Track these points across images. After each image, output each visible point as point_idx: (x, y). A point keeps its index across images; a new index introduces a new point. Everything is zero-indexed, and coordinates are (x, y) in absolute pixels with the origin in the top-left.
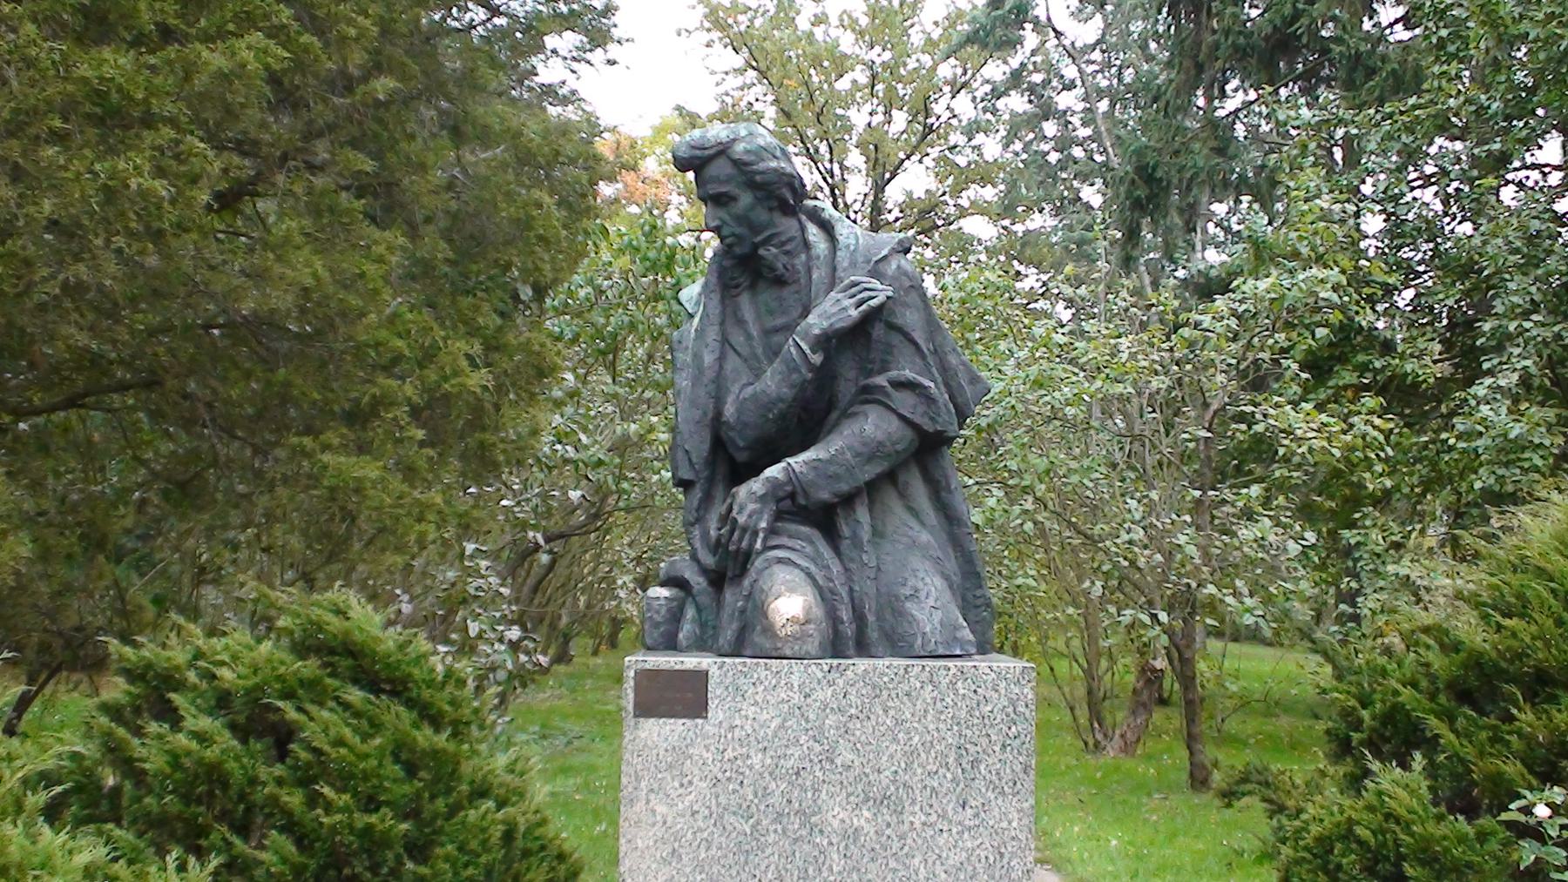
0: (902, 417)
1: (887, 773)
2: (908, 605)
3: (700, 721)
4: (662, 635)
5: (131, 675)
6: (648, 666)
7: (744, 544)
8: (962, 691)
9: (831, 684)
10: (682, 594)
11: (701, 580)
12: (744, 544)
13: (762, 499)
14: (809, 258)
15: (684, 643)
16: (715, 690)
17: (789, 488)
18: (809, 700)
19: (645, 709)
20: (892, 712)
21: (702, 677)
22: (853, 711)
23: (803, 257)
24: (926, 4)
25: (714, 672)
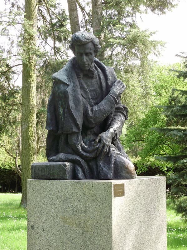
8: (158, 184)
9: (141, 185)
10: (72, 164)
12: (108, 150)
16: (126, 189)
19: (116, 195)
21: (123, 185)
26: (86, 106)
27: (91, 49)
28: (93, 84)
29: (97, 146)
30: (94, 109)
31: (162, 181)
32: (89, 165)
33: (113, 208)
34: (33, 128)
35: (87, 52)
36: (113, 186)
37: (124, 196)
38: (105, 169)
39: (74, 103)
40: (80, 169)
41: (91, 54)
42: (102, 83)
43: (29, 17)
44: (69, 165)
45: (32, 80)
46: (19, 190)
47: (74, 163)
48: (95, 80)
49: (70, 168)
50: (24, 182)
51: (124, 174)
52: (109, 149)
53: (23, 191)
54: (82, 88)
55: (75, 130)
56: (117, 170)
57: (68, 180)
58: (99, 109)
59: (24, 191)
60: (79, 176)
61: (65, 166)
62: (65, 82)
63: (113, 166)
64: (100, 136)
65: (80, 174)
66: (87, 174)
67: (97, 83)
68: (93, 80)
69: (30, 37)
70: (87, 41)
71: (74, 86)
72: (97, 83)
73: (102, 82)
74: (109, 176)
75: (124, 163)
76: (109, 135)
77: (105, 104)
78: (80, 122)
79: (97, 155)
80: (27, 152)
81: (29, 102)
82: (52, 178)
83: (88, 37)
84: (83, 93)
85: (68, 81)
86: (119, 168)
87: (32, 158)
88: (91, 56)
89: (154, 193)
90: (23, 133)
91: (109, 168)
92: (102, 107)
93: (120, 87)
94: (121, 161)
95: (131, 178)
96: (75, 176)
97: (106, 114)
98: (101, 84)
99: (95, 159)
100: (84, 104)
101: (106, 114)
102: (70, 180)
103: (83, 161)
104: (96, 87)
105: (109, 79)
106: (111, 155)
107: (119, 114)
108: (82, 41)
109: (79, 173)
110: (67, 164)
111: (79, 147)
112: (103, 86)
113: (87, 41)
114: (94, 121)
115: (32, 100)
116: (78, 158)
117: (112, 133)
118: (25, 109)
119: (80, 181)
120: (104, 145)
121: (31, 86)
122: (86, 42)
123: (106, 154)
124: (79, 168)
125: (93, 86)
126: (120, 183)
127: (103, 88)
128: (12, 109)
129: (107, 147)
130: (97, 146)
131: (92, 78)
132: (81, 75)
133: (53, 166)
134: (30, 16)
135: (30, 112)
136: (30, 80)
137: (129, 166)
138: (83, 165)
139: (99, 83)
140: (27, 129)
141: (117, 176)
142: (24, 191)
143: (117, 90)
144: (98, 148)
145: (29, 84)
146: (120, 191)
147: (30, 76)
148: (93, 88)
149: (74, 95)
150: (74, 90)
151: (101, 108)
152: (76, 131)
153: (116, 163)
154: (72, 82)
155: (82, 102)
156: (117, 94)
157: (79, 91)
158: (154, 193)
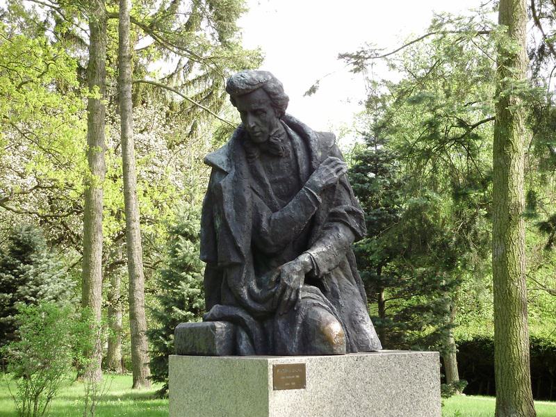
0: (353, 230)
1: (382, 410)
2: (362, 325)
3: (302, 390)
4: (224, 348)
5: (43, 257)
6: (496, 371)
7: (292, 297)
8: (411, 367)
9: (358, 366)
10: (231, 325)
11: (249, 316)
12: (292, 297)
13: (299, 273)
14: (293, 144)
15: (245, 351)
16: (308, 374)
17: (311, 267)
18: (349, 375)
19: (279, 385)
20: (384, 379)
21: (302, 367)
22: (368, 380)
23: (289, 143)
24: (3, 410)
25: (308, 365)
26: (260, 212)
27: (261, 101)
28: (281, 168)
29: (273, 290)
30: (273, 218)
31: (427, 362)
32: (263, 328)
33: (270, 411)
34: (516, 255)
35: (253, 108)
36: (272, 368)
37: (304, 388)
38: (284, 335)
39: (235, 208)
40: (244, 335)
41: (264, 112)
42: (298, 165)
43: (508, 16)
44: (221, 328)
45: (514, 150)
46: (490, 392)
47: (234, 321)
48: (285, 160)
49: (225, 333)
50: (499, 372)
51: (318, 345)
52: (297, 295)
53: (497, 394)
54: (256, 176)
55: (235, 259)
56: (307, 338)
57: (218, 356)
58: (281, 216)
59: (499, 394)
60: (239, 348)
61: (214, 328)
62: (221, 167)
63: (298, 328)
64: (280, 270)
65: (244, 344)
66: (258, 345)
67: (290, 166)
68: (282, 162)
69: (507, 58)
70: (250, 87)
71: (236, 175)
72: (290, 166)
73: (300, 164)
74: (289, 348)
75: (320, 324)
76: (298, 268)
77: (294, 206)
78: (244, 243)
79: (275, 307)
80: (504, 307)
81: (507, 199)
82: (197, 352)
83: (252, 81)
84: (256, 187)
85: (228, 166)
86: (310, 333)
87: (515, 321)
88: (264, 115)
89: (400, 385)
90: (496, 266)
91: (292, 333)
92: (288, 213)
93: (330, 171)
94: (315, 319)
95: (330, 353)
96: (234, 351)
97: (297, 227)
98: (298, 167)
99: (272, 315)
100: (255, 208)
101: (297, 227)
102: (225, 355)
103: (252, 318)
104: (288, 173)
105: (316, 157)
106: (299, 308)
107: (335, 224)
108: (238, 88)
109: (241, 343)
110: (220, 325)
111: (242, 291)
112: (301, 172)
113: (250, 87)
114: (273, 241)
115: (513, 195)
116: (240, 313)
117: (304, 264)
118: (498, 215)
119: (243, 358)
120: (285, 287)
121: (512, 163)
122: (247, 89)
123: (289, 304)
124: (242, 334)
125: (282, 172)
126: (292, 363)
127: (301, 176)
128: (476, 214)
129: (292, 290)
130: (273, 290)
131: (279, 156)
132: (253, 152)
133: (199, 330)
134: (510, 13)
135: (510, 219)
136: (509, 151)
137: (326, 328)
138: (250, 327)
139: (294, 166)
140: (503, 257)
141: (306, 350)
142: (499, 394)
143: (320, 177)
144: (274, 294)
145: (508, 159)
146: (296, 379)
147: (508, 143)
148: (281, 177)
149: (235, 192)
150: (236, 182)
151: (285, 214)
152: (238, 261)
153: (305, 324)
154: (234, 167)
155: (249, 205)
156: (320, 186)
157: (247, 182)
158: (400, 385)
